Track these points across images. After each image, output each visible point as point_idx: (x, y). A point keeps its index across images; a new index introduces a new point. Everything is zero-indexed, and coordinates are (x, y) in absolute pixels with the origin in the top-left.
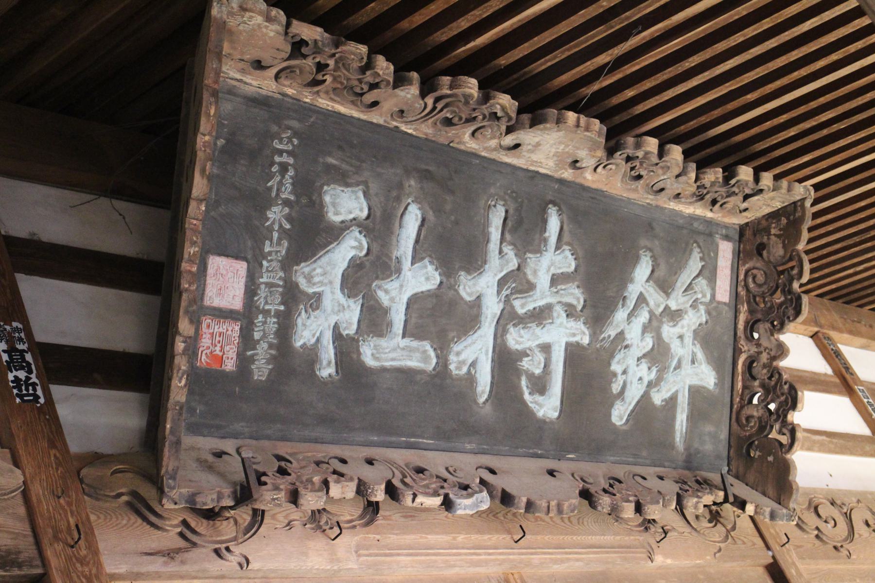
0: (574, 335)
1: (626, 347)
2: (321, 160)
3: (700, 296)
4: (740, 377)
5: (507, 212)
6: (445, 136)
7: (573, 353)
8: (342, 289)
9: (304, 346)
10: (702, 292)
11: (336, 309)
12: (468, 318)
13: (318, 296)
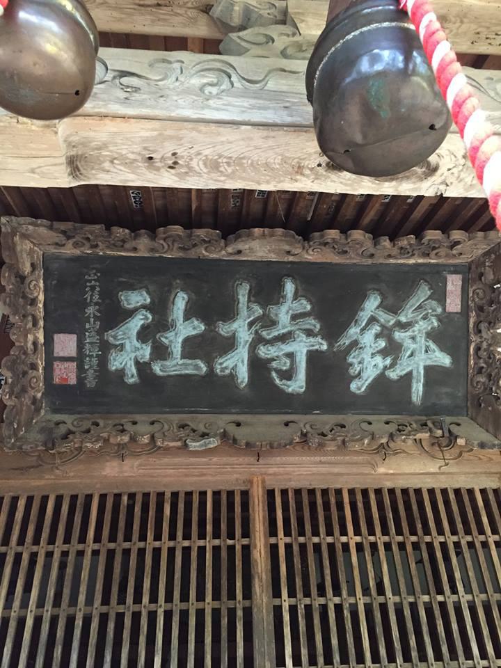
0: (313, 346)
1: (360, 348)
2: (116, 280)
3: (430, 311)
4: (472, 358)
5: (251, 286)
6: (192, 254)
7: (313, 357)
8: (138, 341)
9: (116, 370)
10: (431, 309)
11: (134, 350)
12: (229, 344)
13: (122, 346)
